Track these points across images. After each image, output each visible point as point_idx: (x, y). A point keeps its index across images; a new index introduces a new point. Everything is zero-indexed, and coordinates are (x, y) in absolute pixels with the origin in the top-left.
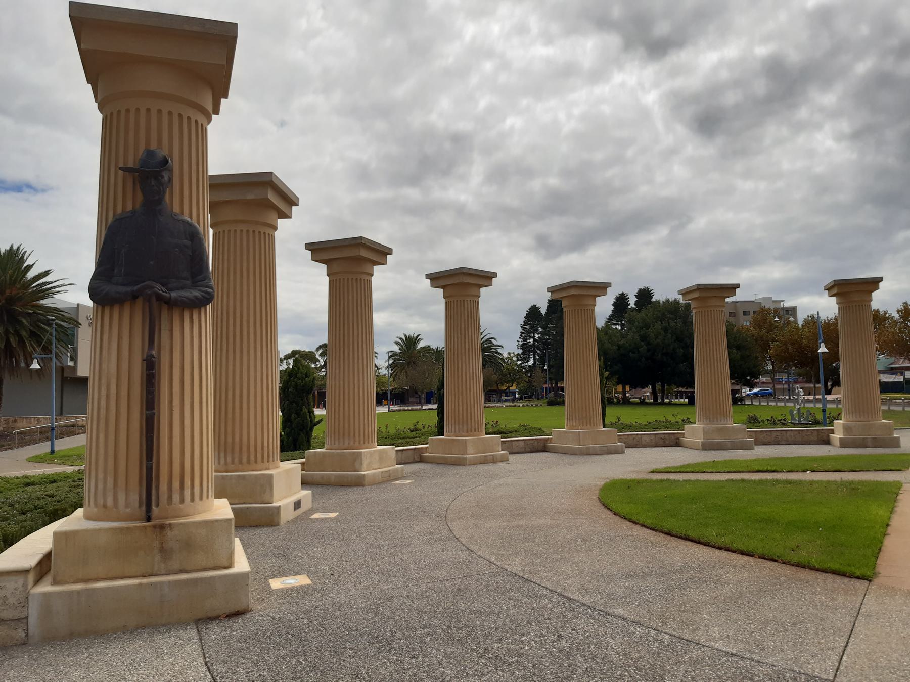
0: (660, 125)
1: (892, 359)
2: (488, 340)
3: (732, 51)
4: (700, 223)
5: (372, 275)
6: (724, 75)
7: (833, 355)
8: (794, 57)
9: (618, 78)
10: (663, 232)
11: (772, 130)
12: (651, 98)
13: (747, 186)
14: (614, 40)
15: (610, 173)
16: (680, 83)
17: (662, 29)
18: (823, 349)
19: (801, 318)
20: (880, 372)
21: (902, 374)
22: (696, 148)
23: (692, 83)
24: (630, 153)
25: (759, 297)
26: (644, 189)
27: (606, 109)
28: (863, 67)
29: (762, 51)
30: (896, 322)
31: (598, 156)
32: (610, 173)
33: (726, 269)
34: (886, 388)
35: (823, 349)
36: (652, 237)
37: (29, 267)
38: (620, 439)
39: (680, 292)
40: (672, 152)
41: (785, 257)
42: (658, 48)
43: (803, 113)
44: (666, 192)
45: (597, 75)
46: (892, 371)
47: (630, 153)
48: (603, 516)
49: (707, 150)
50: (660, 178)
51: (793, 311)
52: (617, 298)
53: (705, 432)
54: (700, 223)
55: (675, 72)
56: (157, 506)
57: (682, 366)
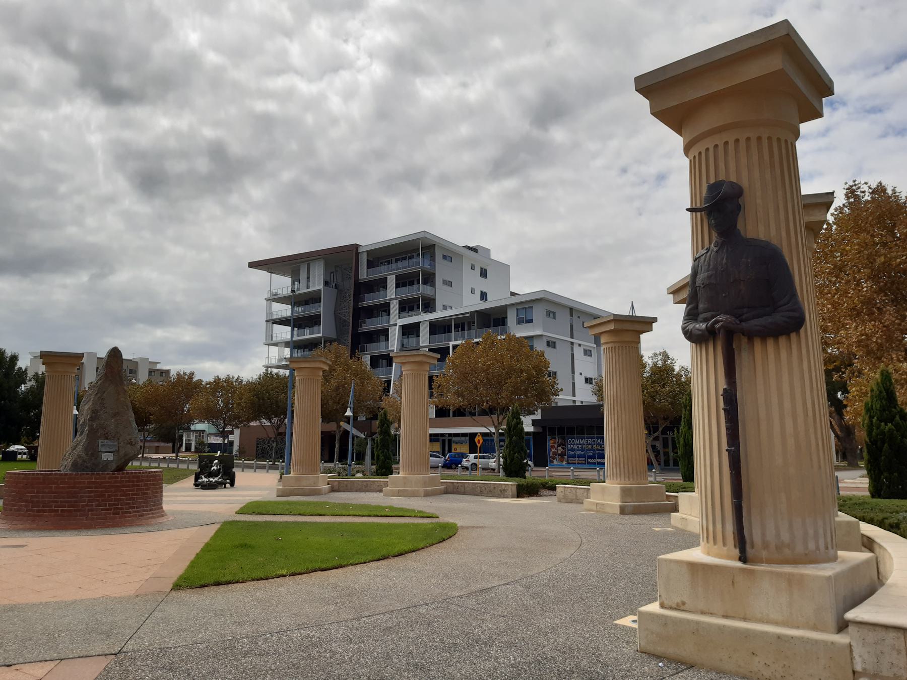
0: (101, 169)
3: (184, 122)
4: (121, 278)
5: (357, 246)
6: (172, 143)
8: (235, 148)
9: (66, 109)
10: (84, 277)
11: (209, 207)
12: (95, 139)
13: (177, 250)
14: (69, 71)
15: (34, 204)
16: (127, 135)
17: (122, 80)
22: (133, 203)
23: (143, 140)
24: (63, 189)
26: (72, 230)
27: (45, 136)
28: (287, 176)
29: (208, 133)
31: (26, 183)
32: (34, 204)
33: (141, 326)
36: (69, 281)
40: (110, 200)
41: (198, 322)
42: (113, 96)
43: (234, 199)
44: (90, 239)
45: (42, 100)
47: (63, 189)
49: (142, 208)
50: (91, 221)
54: (121, 278)
55: (127, 124)
56: (753, 547)
57: (683, 399)
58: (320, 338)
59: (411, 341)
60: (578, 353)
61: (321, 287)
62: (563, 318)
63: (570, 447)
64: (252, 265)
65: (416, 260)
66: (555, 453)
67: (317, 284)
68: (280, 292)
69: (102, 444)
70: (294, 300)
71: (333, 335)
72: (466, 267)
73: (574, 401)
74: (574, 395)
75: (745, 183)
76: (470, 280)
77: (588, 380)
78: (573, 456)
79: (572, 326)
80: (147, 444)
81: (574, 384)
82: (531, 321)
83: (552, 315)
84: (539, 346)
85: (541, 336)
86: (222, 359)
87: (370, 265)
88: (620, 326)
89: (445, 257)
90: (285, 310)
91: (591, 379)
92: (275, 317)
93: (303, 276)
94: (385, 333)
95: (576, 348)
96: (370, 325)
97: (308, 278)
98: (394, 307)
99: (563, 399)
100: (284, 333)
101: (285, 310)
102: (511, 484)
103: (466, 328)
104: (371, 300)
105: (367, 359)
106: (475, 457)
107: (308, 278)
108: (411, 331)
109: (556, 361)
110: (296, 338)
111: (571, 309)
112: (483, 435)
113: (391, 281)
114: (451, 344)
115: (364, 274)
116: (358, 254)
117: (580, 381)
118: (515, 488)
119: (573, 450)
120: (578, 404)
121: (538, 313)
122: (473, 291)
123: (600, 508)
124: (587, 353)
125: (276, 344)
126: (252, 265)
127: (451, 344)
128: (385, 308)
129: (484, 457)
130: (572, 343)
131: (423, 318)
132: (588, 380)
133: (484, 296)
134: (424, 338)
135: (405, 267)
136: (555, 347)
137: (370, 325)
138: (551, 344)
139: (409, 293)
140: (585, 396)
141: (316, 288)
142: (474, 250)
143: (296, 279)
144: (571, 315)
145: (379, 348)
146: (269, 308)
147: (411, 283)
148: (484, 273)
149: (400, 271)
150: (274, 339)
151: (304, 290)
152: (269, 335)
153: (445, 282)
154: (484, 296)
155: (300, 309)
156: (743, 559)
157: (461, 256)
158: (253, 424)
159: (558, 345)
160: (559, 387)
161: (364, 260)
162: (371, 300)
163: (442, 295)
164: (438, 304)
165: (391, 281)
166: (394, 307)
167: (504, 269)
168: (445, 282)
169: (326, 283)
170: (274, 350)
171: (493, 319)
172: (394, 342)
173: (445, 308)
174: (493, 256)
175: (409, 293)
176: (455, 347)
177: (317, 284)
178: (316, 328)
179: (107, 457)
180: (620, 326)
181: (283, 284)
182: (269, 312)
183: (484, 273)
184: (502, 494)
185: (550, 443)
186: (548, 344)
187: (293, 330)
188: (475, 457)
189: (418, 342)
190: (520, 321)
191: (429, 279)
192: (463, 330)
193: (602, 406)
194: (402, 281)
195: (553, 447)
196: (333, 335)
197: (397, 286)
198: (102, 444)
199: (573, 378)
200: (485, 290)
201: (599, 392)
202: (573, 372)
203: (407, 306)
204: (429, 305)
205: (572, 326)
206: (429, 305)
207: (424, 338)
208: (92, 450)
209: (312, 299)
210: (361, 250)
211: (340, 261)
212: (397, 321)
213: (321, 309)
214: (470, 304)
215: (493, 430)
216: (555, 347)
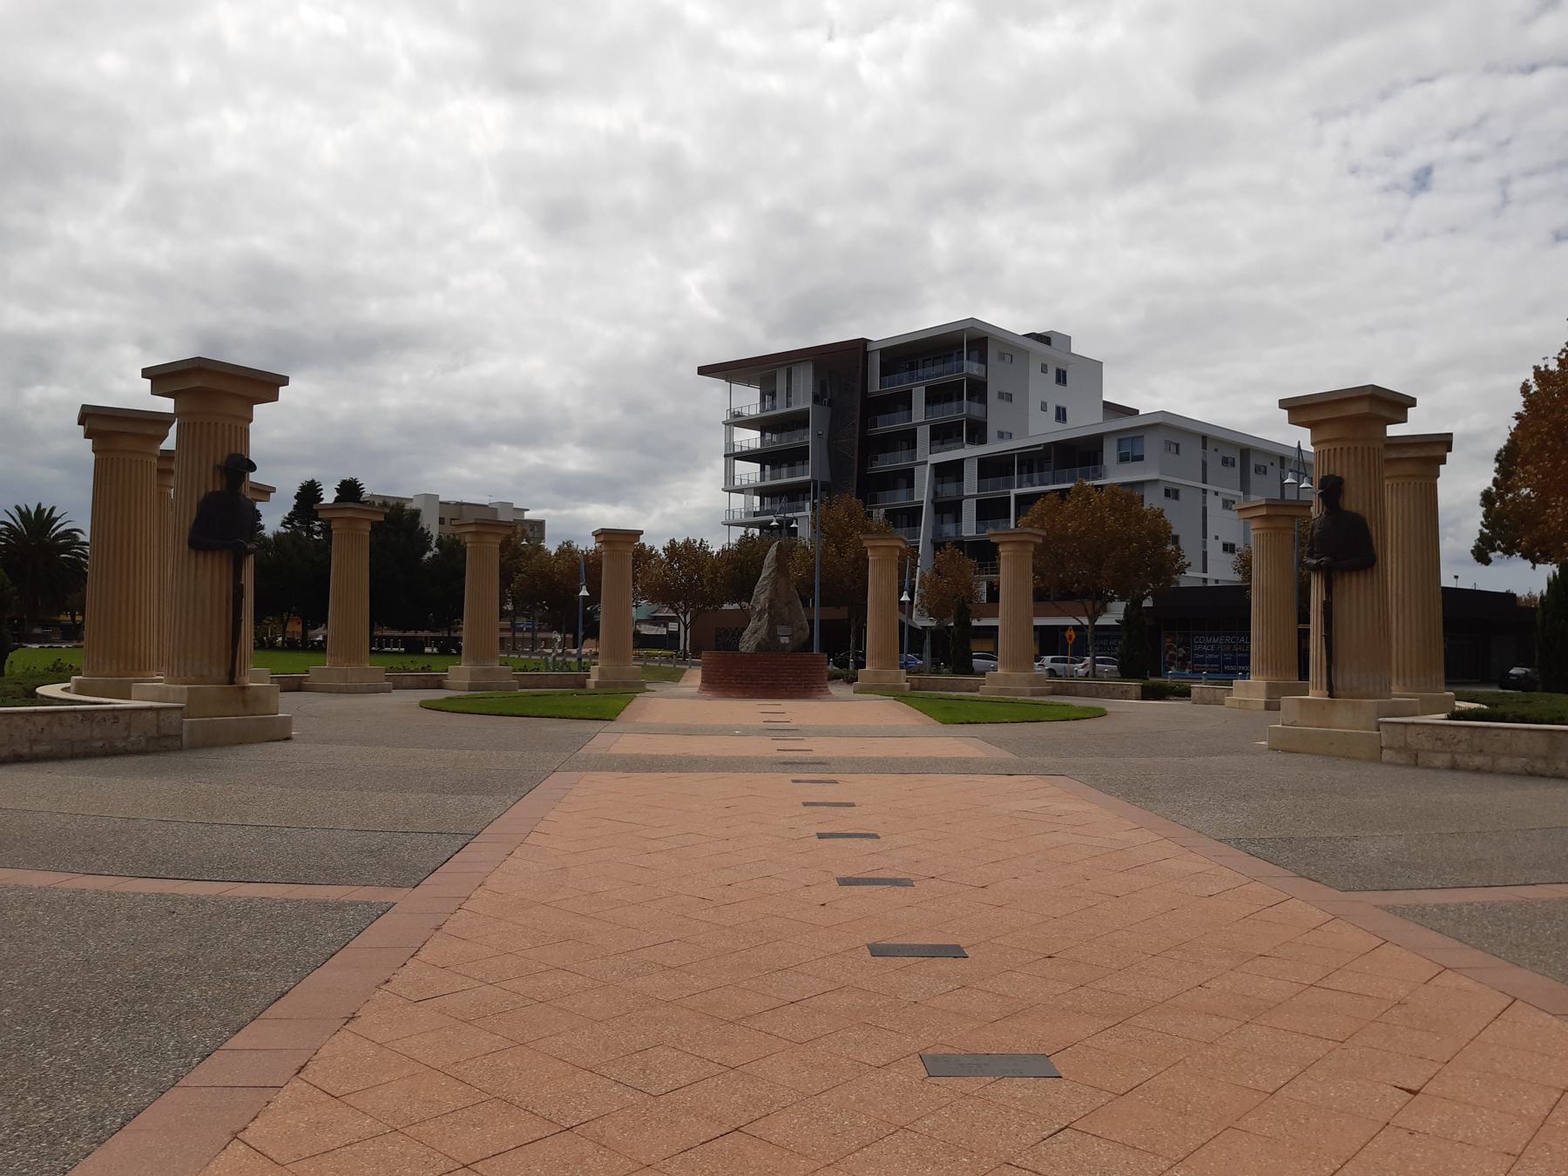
1: (655, 607)
2: (68, 532)
5: (864, 342)
7: (595, 597)
17: (546, 62)
18: (584, 592)
19: (551, 546)
20: (639, 622)
21: (666, 626)
25: (493, 500)
30: (662, 562)
34: (642, 641)
35: (584, 592)
37: (56, 519)
38: (388, 678)
39: (160, 378)
42: (518, 84)
46: (655, 621)
48: (1451, 530)
51: (539, 525)
52: (302, 488)
53: (472, 673)
58: (808, 482)
59: (949, 490)
60: (1214, 505)
61: (809, 405)
62: (1192, 451)
63: (1197, 648)
64: (703, 371)
65: (956, 364)
66: (1173, 657)
67: (803, 400)
68: (745, 412)
69: (781, 629)
70: (762, 424)
71: (827, 478)
72: (1034, 369)
73: (1205, 580)
74: (1205, 571)
75: (1345, 476)
76: (1041, 388)
77: (1228, 548)
78: (1202, 661)
79: (1204, 465)
80: (518, 635)
81: (1205, 554)
82: (1141, 458)
83: (1173, 448)
84: (1153, 500)
85: (1156, 481)
86: (613, 500)
87: (886, 370)
88: (1272, 512)
89: (1002, 356)
90: (750, 439)
91: (1233, 546)
92: (737, 450)
93: (781, 386)
94: (908, 477)
95: (1210, 496)
96: (886, 463)
97: (789, 395)
98: (923, 435)
99: (1191, 578)
100: (749, 472)
101: (750, 439)
102: (1134, 685)
103: (1036, 466)
104: (886, 425)
105: (879, 514)
106: (1053, 661)
107: (789, 395)
108: (949, 472)
109: (1179, 519)
110: (768, 482)
111: (1204, 438)
112: (1075, 628)
113: (919, 395)
114: (1014, 492)
115: (875, 385)
116: (866, 354)
117: (1214, 549)
118: (1139, 690)
119: (1201, 652)
120: (1210, 584)
121: (1152, 447)
122: (1044, 407)
123: (1243, 705)
124: (1227, 504)
125: (740, 491)
126: (703, 371)
127: (1014, 492)
128: (909, 438)
129: (1065, 661)
130: (1205, 491)
131: (968, 452)
132: (1228, 548)
133: (1061, 414)
134: (971, 482)
135: (939, 374)
136: (1176, 498)
137: (886, 463)
138: (1172, 493)
139: (948, 413)
140: (1222, 571)
141: (801, 406)
142: (1044, 339)
143: (768, 393)
144: (1204, 447)
145: (899, 499)
146: (730, 435)
147: (949, 399)
148: (1061, 377)
149: (933, 381)
150: (737, 483)
151: (781, 410)
152: (729, 475)
153: (1001, 396)
154: (1061, 414)
155: (775, 437)
156: (1331, 696)
157: (1026, 353)
158: (726, 606)
159: (1181, 495)
160: (1186, 561)
161: (875, 363)
162: (886, 425)
163: (997, 416)
164: (992, 432)
165: (919, 395)
166: (923, 435)
167: (1094, 369)
168: (1001, 396)
169: (816, 399)
170: (739, 501)
171: (1080, 454)
172: (923, 490)
173: (1001, 435)
174: (1076, 349)
175: (948, 413)
176: (1017, 496)
177: (803, 400)
178: (799, 468)
179: (785, 640)
180: (1272, 512)
181: (749, 399)
182: (730, 443)
183: (1061, 377)
184: (1125, 695)
185: (1167, 642)
186: (1167, 493)
187: (762, 469)
188: (1053, 661)
189: (960, 489)
190: (1123, 458)
191: (978, 390)
192: (1030, 471)
193: (1249, 587)
194: (935, 396)
195: (1170, 648)
196: (827, 478)
197: (928, 402)
198: (781, 629)
199: (1205, 545)
200: (1062, 404)
201: (1245, 567)
202: (1205, 536)
203: (943, 434)
204: (977, 432)
205: (1204, 465)
206: (977, 432)
207: (971, 482)
208: (772, 635)
209: (796, 421)
210: (870, 348)
211: (839, 365)
212: (928, 457)
213: (809, 437)
214: (1041, 430)
215: (1086, 621)
216: (1176, 498)
